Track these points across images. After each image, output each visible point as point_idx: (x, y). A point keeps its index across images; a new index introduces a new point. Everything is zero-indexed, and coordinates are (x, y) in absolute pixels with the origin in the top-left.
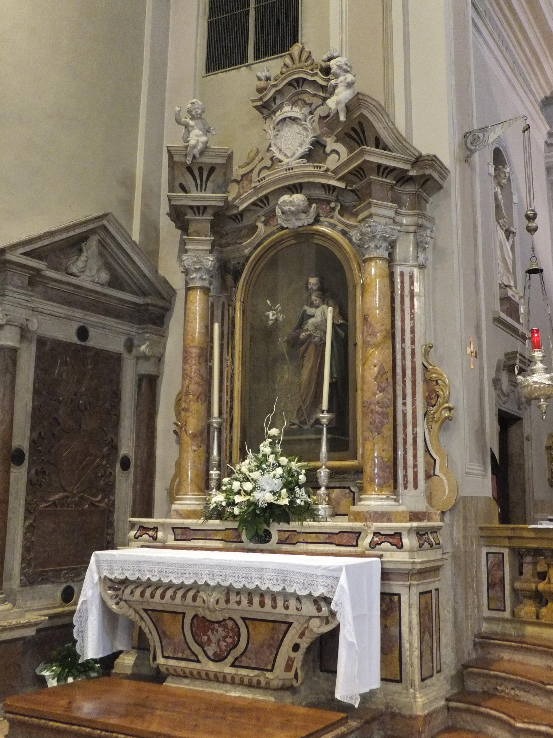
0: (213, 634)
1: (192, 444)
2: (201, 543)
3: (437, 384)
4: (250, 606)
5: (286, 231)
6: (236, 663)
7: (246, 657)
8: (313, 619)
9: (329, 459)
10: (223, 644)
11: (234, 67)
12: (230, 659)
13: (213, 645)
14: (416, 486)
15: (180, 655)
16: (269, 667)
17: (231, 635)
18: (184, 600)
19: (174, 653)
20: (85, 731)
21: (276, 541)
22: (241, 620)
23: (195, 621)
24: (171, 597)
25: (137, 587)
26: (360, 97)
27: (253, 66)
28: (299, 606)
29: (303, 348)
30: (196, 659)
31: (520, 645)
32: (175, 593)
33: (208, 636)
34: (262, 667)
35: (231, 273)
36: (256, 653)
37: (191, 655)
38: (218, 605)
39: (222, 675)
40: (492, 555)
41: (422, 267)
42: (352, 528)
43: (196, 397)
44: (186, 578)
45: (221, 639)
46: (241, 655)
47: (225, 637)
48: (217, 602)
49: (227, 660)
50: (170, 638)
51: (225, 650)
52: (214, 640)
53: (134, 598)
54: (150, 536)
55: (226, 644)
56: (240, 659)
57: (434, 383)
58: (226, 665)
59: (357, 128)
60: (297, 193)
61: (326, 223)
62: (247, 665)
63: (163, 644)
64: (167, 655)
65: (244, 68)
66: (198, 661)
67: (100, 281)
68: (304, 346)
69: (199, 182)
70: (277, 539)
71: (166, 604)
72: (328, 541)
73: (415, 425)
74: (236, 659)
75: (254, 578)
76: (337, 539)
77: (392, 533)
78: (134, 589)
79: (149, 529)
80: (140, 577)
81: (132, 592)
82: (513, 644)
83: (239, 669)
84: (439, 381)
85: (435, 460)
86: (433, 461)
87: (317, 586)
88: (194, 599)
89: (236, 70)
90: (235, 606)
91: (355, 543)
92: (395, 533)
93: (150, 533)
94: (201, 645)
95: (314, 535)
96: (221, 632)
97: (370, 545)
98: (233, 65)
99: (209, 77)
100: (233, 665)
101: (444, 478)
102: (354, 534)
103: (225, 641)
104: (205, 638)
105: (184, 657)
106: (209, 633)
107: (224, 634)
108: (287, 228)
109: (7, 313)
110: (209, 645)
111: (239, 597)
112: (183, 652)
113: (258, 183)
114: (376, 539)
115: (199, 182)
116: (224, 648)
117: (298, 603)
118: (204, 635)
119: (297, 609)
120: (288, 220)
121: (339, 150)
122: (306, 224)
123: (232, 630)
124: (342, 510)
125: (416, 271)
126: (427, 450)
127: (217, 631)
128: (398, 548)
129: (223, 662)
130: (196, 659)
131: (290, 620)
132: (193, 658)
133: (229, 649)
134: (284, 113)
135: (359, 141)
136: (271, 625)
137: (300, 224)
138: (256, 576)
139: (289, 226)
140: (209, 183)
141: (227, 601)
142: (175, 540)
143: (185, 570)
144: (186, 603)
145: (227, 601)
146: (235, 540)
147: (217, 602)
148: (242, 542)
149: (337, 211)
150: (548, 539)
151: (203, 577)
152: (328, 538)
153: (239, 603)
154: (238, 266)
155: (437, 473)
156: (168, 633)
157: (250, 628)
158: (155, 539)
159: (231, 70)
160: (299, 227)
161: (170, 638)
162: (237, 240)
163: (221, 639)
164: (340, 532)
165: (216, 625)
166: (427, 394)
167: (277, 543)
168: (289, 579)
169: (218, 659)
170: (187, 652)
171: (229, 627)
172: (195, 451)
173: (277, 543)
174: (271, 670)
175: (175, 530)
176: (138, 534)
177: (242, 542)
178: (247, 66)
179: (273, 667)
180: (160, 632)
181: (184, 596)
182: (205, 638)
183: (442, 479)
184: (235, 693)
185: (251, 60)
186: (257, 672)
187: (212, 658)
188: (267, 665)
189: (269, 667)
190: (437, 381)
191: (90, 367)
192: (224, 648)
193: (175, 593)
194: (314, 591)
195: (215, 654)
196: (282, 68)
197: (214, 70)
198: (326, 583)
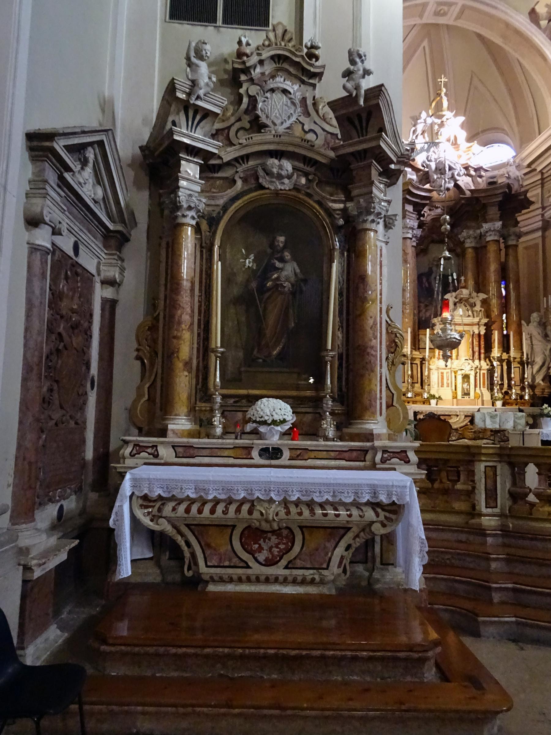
0: (264, 542)
1: (184, 370)
2: (207, 460)
3: (396, 336)
4: (312, 516)
5: (267, 191)
6: (290, 566)
7: (300, 559)
8: (375, 523)
9: (222, 388)
10: (275, 551)
11: (202, 23)
12: (283, 562)
13: (265, 551)
14: (381, 414)
15: (227, 563)
16: (325, 566)
17: (285, 542)
18: (238, 514)
19: (220, 562)
20: (223, 652)
21: (288, 458)
22: (298, 529)
23: (246, 532)
24: (223, 512)
25: (179, 504)
26: (383, 89)
27: (221, 29)
28: (361, 514)
29: (267, 295)
30: (245, 565)
31: (436, 527)
32: (227, 508)
33: (260, 545)
34: (317, 566)
35: (206, 218)
36: (311, 555)
37: (240, 563)
38: (278, 517)
39: (274, 577)
40: (489, 468)
41: (387, 243)
42: (361, 447)
43: (188, 327)
44: (219, 494)
45: (274, 546)
46: (295, 558)
47: (279, 544)
48: (277, 515)
49: (279, 564)
50: (215, 550)
51: (278, 555)
52: (265, 547)
53: (179, 514)
54: (149, 454)
55: (278, 550)
56: (293, 562)
57: (394, 335)
58: (278, 567)
59: (364, 116)
60: (276, 158)
61: (303, 192)
62: (302, 566)
63: (206, 555)
64: (211, 564)
65: (213, 28)
66: (248, 567)
67: (95, 198)
68: (270, 293)
69: (190, 123)
70: (289, 456)
71: (217, 518)
72: (338, 457)
73: (381, 367)
74: (289, 562)
75: (323, 492)
76: (346, 455)
77: (399, 451)
78: (176, 505)
79: (148, 447)
80: (149, 494)
81: (174, 509)
82: (430, 527)
83: (293, 570)
84: (398, 335)
85: (393, 394)
86: (391, 395)
87: (238, 490)
88: (250, 512)
89: (204, 27)
90: (297, 517)
91: (363, 459)
92: (402, 451)
93: (149, 450)
94: (251, 552)
95: (325, 453)
96: (274, 540)
97: (381, 461)
98: (200, 21)
99: (172, 24)
100: (286, 567)
101: (400, 408)
102: (362, 452)
103: (277, 547)
104: (257, 546)
105: (232, 564)
106: (261, 542)
107: (277, 541)
108: (268, 188)
109: (51, 211)
110: (260, 552)
111: (299, 508)
112: (230, 560)
113: (245, 141)
114: (385, 456)
115: (190, 123)
116: (276, 553)
117: (360, 511)
118: (254, 544)
119: (360, 516)
120: (272, 182)
121: (316, 130)
122: (287, 189)
123: (287, 537)
124: (230, 430)
125: (383, 245)
126: (387, 387)
127: (270, 539)
128: (405, 462)
129: (275, 566)
130: (245, 565)
131: (350, 526)
132: (242, 564)
133: (281, 554)
134: (276, 83)
135: (359, 128)
136: (329, 531)
137: (283, 188)
138: (367, 492)
139: (270, 187)
140: (198, 127)
141: (288, 513)
142: (176, 457)
143: (176, 485)
144: (240, 516)
145: (288, 513)
146: (245, 457)
147: (277, 515)
148: (253, 459)
149: (315, 184)
150: (548, 457)
151: (253, 492)
152: (339, 454)
153: (300, 514)
154: (212, 212)
155: (394, 404)
156: (213, 545)
157: (306, 534)
158: (156, 456)
159: (198, 25)
160: (281, 190)
161: (215, 550)
162: (211, 189)
163: (274, 546)
164: (349, 450)
165: (269, 535)
166: (388, 343)
167: (289, 460)
168: (360, 491)
169: (270, 563)
170: (235, 560)
171: (284, 535)
172: (186, 376)
173: (289, 460)
174: (327, 569)
175: (176, 448)
176: (134, 452)
177: (253, 459)
178: (215, 27)
179: (328, 565)
180: (203, 544)
181: (238, 510)
182: (257, 546)
183: (398, 409)
184: (288, 590)
185: (220, 22)
186: (311, 571)
187: (264, 563)
188: (322, 564)
189: (325, 566)
190: (396, 334)
191: (79, 284)
192: (276, 553)
193: (227, 508)
194: (290, 496)
195: (266, 559)
196: (264, 41)
197: (179, 18)
198: (246, 487)
